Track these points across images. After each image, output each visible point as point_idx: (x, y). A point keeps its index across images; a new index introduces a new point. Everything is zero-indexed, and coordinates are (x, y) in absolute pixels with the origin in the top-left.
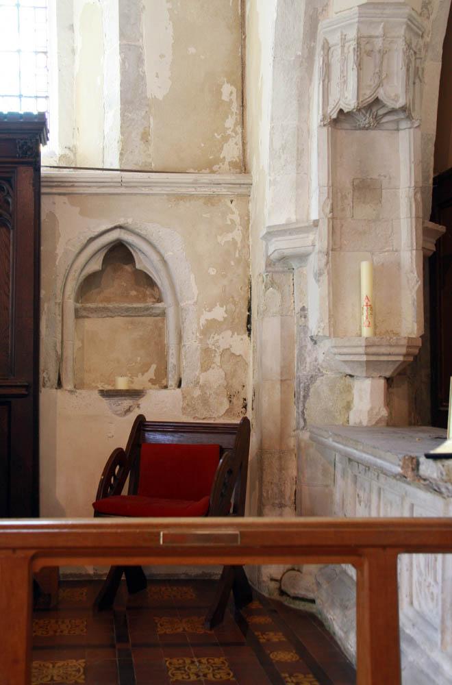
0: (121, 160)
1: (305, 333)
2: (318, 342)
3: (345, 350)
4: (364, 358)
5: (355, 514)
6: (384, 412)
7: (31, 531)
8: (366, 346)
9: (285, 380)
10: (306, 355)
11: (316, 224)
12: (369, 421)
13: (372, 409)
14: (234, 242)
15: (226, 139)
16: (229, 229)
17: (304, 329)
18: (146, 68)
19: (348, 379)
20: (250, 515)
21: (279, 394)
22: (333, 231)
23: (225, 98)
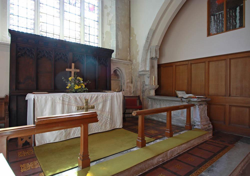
0: (116, 57)
5: (6, 44)
11: (149, 71)
14: (130, 71)
15: (128, 56)
16: (129, 69)
18: (119, 44)
20: (66, 114)
22: (151, 72)
23: (128, 50)
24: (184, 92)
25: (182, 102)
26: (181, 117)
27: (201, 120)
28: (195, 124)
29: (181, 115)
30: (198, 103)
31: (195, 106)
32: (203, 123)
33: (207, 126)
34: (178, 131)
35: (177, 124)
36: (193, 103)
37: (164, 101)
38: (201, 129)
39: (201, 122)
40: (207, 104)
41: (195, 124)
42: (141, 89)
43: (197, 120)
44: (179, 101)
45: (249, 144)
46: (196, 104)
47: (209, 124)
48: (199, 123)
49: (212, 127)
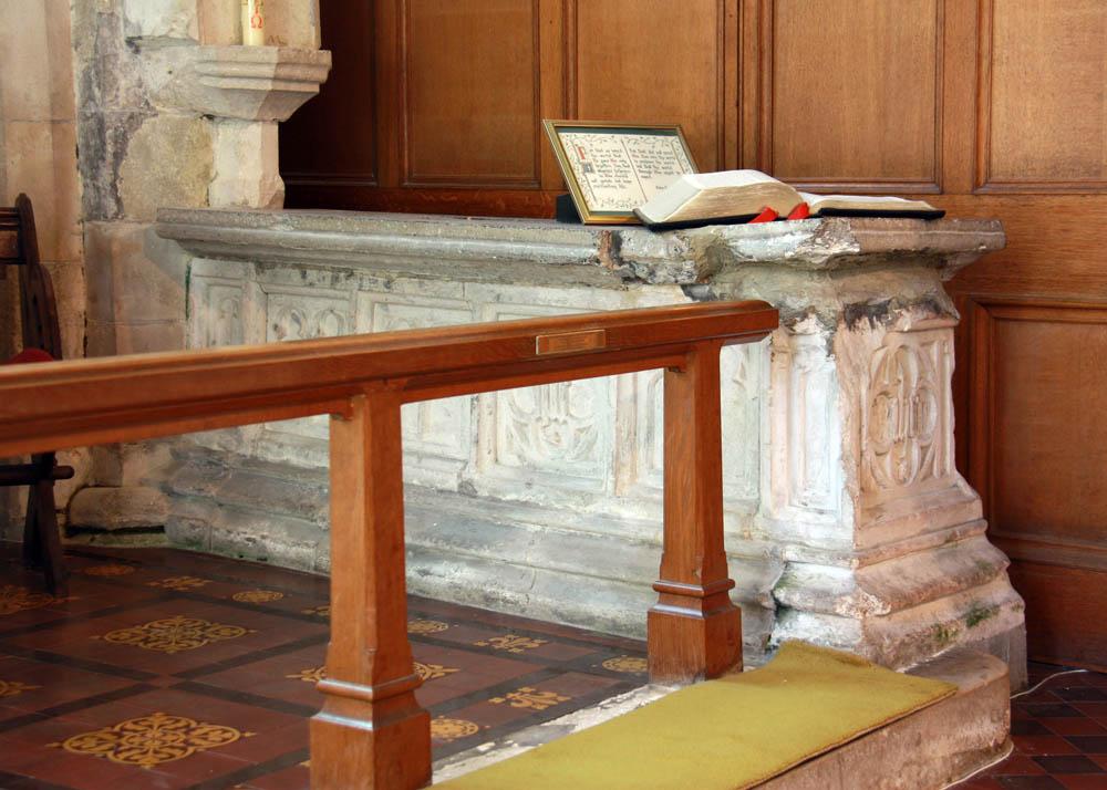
1: (114, 29)
2: (143, 49)
3: (235, 69)
4: (268, 86)
6: (280, 185)
7: (114, 376)
8: (278, 64)
9: (59, 122)
10: (116, 72)
12: (262, 199)
13: (264, 177)
17: (110, 23)
19: (206, 123)
21: (51, 150)
24: (671, 146)
25: (627, 279)
26: (617, 495)
27: (860, 527)
28: (781, 595)
29: (616, 470)
30: (824, 294)
31: (792, 334)
32: (884, 569)
33: (943, 611)
34: (548, 698)
35: (569, 606)
36: (756, 289)
37: (388, 284)
38: (866, 653)
39: (865, 557)
40: (948, 305)
41: (782, 583)
42: (59, 99)
43: (816, 535)
44: (581, 262)
45: (377, 785)
46: (795, 304)
47: (978, 576)
48: (839, 576)
49: (1020, 617)
